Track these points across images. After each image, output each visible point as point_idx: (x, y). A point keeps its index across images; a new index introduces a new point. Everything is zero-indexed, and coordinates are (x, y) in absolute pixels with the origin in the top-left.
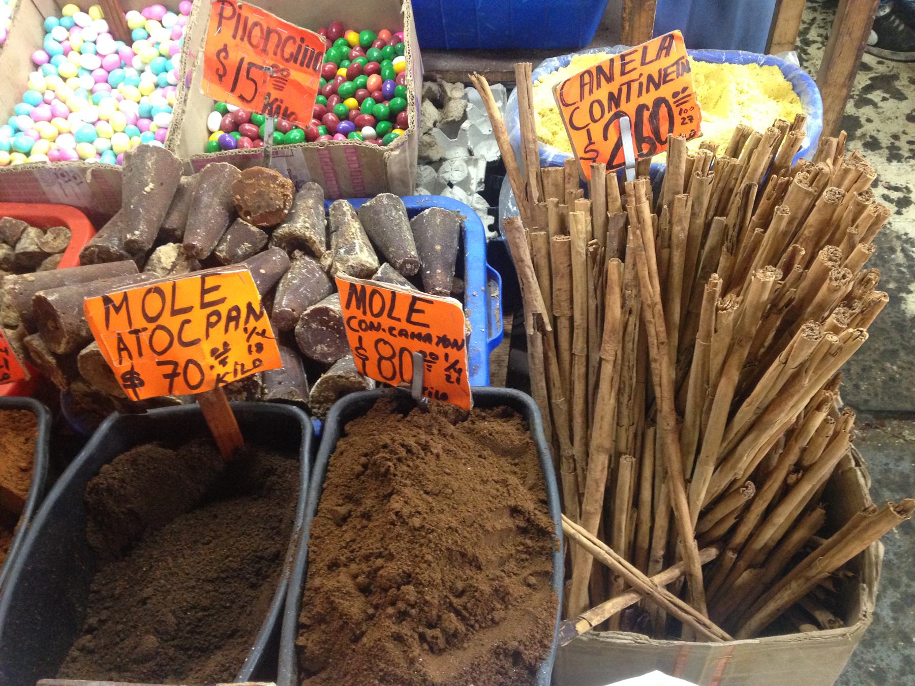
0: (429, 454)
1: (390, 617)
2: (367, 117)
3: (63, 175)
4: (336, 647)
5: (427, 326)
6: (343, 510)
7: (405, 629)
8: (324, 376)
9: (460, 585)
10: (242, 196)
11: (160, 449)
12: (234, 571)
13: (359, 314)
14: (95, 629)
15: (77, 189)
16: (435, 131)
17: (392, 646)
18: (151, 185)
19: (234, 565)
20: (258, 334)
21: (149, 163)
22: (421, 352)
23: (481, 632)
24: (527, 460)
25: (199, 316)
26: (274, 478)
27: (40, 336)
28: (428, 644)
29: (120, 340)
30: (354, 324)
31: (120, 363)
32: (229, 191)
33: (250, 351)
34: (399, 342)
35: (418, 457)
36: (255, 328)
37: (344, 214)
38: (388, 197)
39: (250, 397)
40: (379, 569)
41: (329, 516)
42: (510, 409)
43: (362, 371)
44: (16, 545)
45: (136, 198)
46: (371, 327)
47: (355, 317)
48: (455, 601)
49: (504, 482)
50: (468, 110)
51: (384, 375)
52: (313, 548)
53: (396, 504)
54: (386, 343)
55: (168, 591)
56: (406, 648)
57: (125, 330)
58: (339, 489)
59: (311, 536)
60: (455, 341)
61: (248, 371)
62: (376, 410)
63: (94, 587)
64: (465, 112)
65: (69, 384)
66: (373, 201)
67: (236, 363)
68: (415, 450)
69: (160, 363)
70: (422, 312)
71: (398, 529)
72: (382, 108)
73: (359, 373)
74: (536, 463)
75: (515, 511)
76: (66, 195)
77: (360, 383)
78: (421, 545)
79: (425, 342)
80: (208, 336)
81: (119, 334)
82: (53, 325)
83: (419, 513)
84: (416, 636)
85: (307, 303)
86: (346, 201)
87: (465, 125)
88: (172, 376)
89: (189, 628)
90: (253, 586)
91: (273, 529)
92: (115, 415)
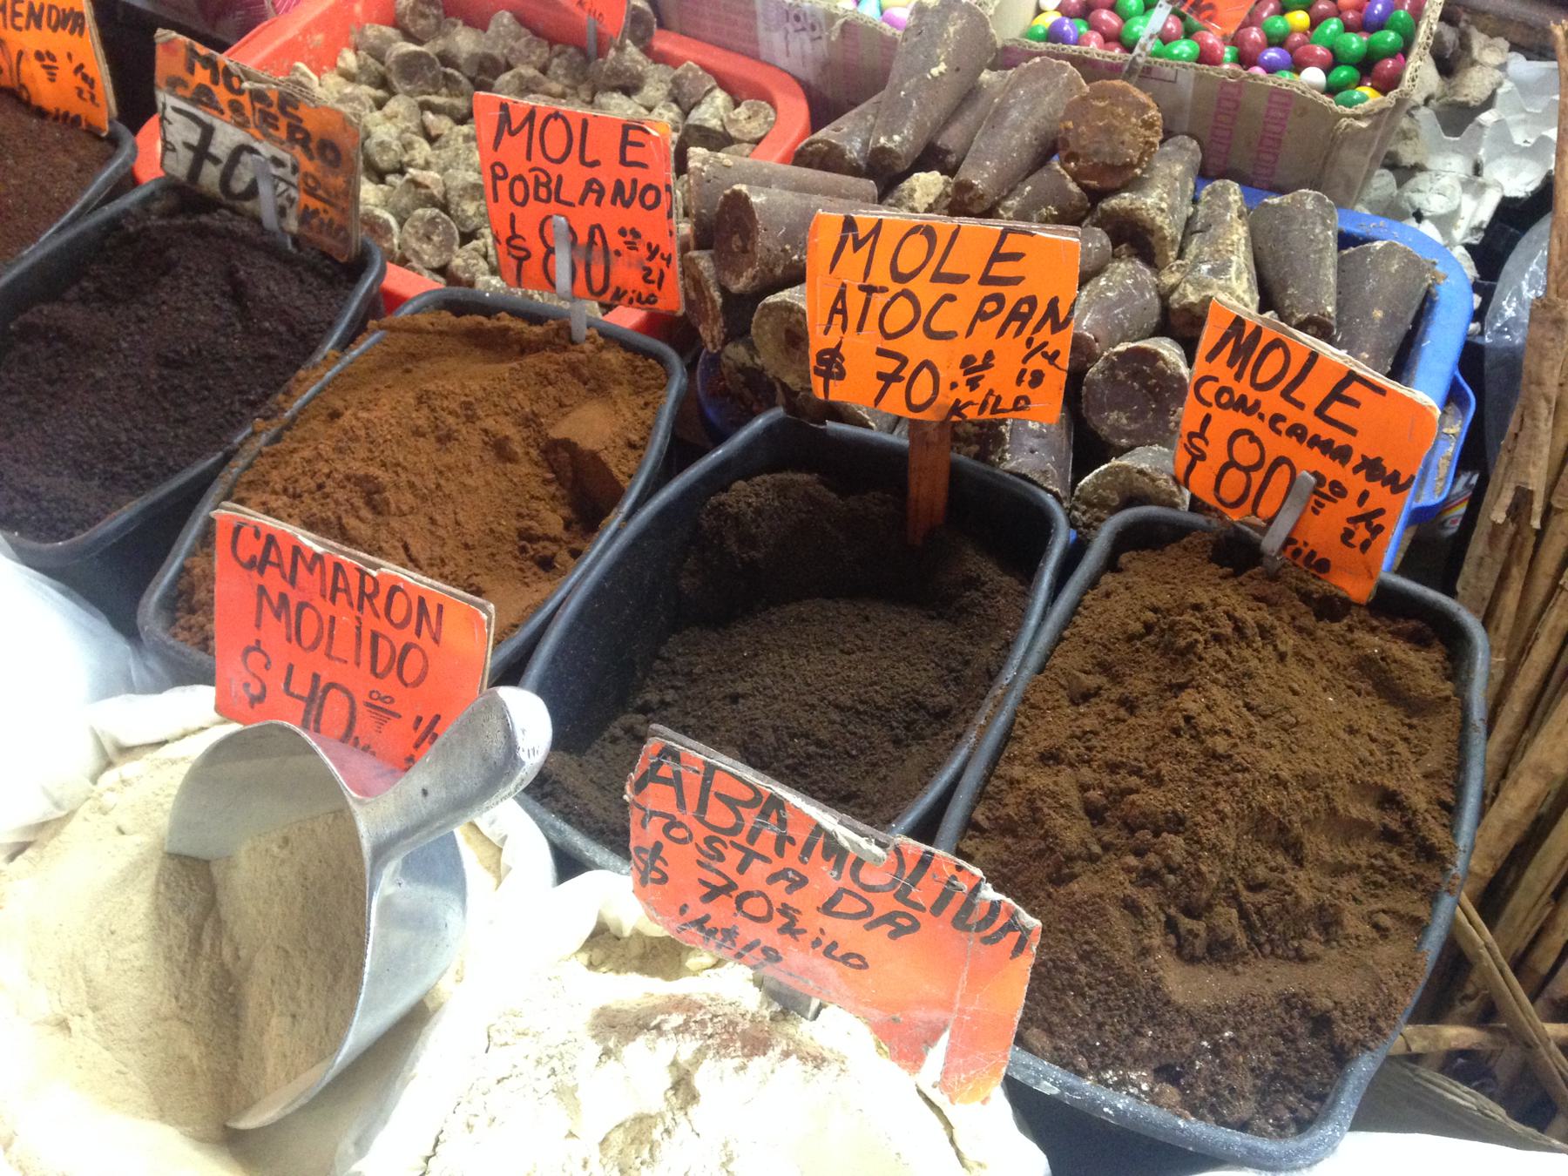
0: (1270, 648)
1: (1128, 870)
2: (1320, 51)
3: (797, 18)
4: (1021, 878)
5: (1352, 431)
6: (1091, 681)
7: (1147, 899)
8: (1114, 462)
9: (1261, 872)
10: (1077, 126)
11: (822, 487)
12: (878, 708)
13: (1226, 376)
14: (652, 710)
15: (808, 47)
16: (1425, 114)
17: (1118, 914)
18: (942, 67)
19: (881, 702)
20: (1045, 355)
21: (951, 30)
22: (1315, 474)
23: (1271, 960)
24: (1436, 728)
25: (971, 294)
26: (976, 595)
27: (712, 256)
28: (1178, 937)
29: (841, 295)
30: (1209, 391)
31: (826, 332)
32: (1056, 112)
33: (1019, 381)
34: (1278, 445)
35: (1249, 646)
36: (1045, 344)
37: (1227, 206)
38: (1319, 200)
39: (982, 457)
40: (1131, 791)
41: (1063, 682)
42: (1429, 631)
43: (1181, 477)
44: (599, 546)
45: (914, 80)
46: (1241, 405)
47: (1216, 379)
48: (1245, 895)
49: (1389, 748)
50: (1500, 91)
51: (343, 696)
52: (1022, 719)
53: (1190, 702)
54: (1253, 439)
55: (775, 697)
56: (1140, 928)
57: (854, 280)
58: (1091, 649)
59: (1024, 700)
60: (1396, 475)
61: (1003, 411)
62: (1185, 549)
63: (663, 651)
64: (1493, 94)
65: (725, 343)
66: (1287, 198)
67: (991, 392)
68: (1249, 632)
69: (881, 352)
70: (1356, 404)
71: (1184, 743)
72: (1355, 43)
73: (1175, 479)
74: (1454, 737)
75: (1389, 800)
76: (788, 54)
77: (1172, 494)
78: (1218, 784)
79: (1333, 458)
80: (969, 332)
81: (844, 285)
82: (740, 243)
83: (1228, 733)
84: (1163, 918)
85: (1119, 336)
86: (1236, 186)
87: (1487, 117)
88: (888, 379)
89: (790, 761)
90: (897, 742)
91: (951, 671)
92: (778, 412)
